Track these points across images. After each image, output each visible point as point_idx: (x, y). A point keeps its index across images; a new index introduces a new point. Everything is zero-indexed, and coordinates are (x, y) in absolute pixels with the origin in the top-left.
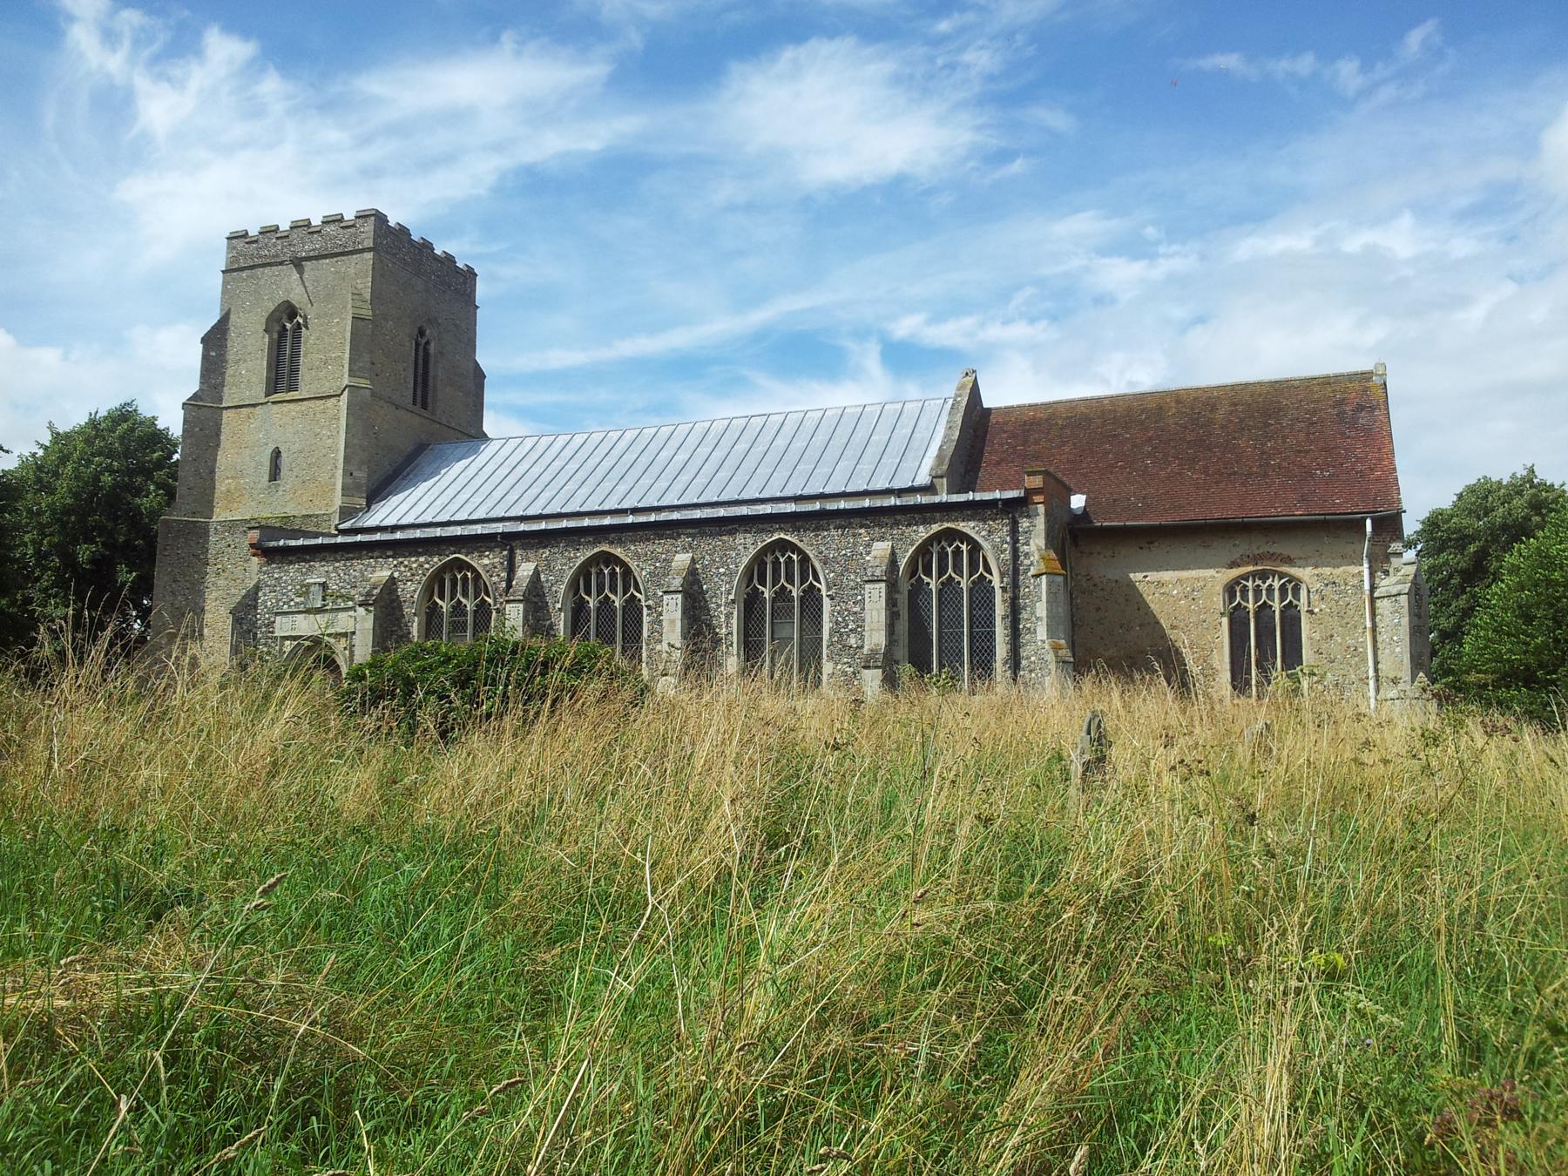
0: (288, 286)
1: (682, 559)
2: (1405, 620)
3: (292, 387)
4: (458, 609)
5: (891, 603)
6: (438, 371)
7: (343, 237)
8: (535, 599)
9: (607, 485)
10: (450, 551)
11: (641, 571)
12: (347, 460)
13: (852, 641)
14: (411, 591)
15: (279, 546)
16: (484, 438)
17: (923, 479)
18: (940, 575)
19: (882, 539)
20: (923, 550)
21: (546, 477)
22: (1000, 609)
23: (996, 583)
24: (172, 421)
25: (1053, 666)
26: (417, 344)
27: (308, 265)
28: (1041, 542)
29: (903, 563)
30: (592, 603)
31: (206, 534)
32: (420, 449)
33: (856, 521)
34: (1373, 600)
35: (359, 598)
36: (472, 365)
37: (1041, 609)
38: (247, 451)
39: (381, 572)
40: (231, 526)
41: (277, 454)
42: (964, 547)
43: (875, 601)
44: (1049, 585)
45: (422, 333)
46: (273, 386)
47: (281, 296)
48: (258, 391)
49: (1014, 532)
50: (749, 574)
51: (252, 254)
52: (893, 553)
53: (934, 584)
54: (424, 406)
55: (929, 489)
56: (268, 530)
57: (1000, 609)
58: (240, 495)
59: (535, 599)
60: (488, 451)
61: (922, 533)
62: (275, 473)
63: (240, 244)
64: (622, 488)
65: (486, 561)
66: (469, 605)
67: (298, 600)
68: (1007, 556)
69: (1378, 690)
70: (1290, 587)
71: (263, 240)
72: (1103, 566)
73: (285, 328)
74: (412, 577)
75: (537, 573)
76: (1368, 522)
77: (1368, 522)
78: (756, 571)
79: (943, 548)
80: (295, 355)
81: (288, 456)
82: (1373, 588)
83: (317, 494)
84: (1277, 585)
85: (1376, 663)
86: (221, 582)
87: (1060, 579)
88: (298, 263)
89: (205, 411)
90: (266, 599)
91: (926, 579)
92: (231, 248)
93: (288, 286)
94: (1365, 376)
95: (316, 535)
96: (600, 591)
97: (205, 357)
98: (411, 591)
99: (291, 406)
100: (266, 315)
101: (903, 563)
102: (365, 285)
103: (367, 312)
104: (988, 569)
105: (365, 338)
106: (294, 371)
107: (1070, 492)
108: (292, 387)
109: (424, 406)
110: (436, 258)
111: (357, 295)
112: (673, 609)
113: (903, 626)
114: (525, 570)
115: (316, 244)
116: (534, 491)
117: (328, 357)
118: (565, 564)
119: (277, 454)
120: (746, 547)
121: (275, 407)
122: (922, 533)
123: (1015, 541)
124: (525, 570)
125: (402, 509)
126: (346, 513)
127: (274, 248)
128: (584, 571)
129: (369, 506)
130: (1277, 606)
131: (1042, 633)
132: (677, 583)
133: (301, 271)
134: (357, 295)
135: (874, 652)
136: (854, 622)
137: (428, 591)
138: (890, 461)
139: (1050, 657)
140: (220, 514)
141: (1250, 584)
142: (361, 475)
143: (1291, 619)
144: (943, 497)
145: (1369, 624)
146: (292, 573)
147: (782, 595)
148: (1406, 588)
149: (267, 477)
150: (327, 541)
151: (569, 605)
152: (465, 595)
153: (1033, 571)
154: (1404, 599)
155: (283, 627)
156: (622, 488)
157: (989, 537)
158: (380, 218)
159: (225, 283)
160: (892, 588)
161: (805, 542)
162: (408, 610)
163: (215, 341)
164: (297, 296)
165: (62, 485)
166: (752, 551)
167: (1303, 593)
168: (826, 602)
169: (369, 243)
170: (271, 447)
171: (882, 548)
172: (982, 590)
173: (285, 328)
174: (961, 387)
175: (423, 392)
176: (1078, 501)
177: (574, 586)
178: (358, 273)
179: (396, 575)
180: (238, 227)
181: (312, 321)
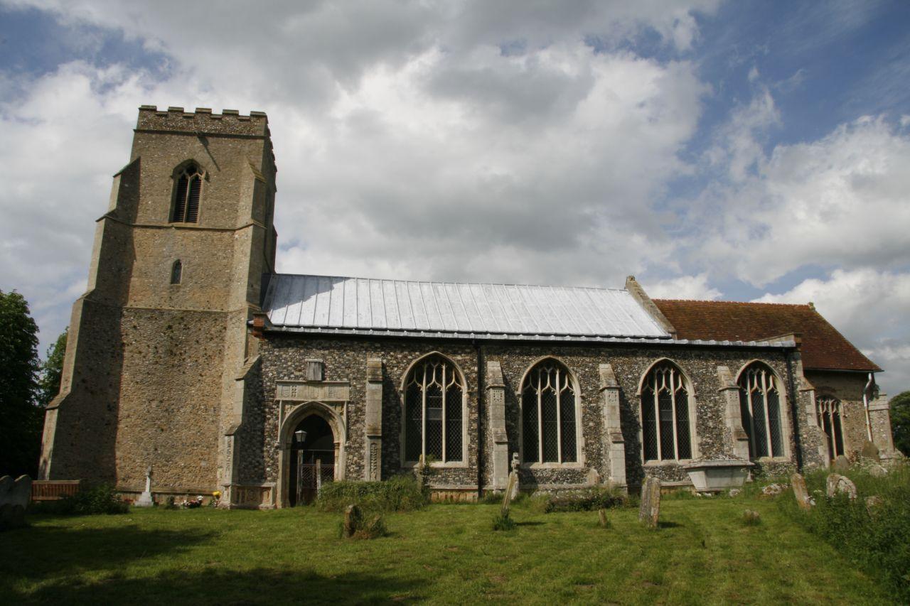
3: (191, 217)
7: (239, 128)
13: (711, 424)
33: (706, 353)
36: (272, 228)
38: (152, 259)
41: (177, 266)
46: (176, 216)
47: (186, 156)
48: (162, 217)
49: (789, 367)
53: (424, 389)
61: (534, 362)
62: (175, 278)
63: (151, 116)
65: (459, 358)
67: (298, 373)
70: (836, 403)
71: (171, 116)
79: (544, 370)
84: (830, 402)
88: (203, 137)
90: (270, 371)
91: (419, 385)
99: (192, 232)
108: (194, 221)
115: (218, 126)
119: (177, 266)
121: (179, 232)
122: (416, 358)
127: (180, 123)
133: (206, 144)
140: (130, 304)
145: (868, 423)
148: (887, 407)
149: (168, 280)
154: (886, 412)
155: (283, 393)
163: (129, 178)
164: (201, 156)
170: (174, 259)
177: (410, 378)
179: (385, 361)
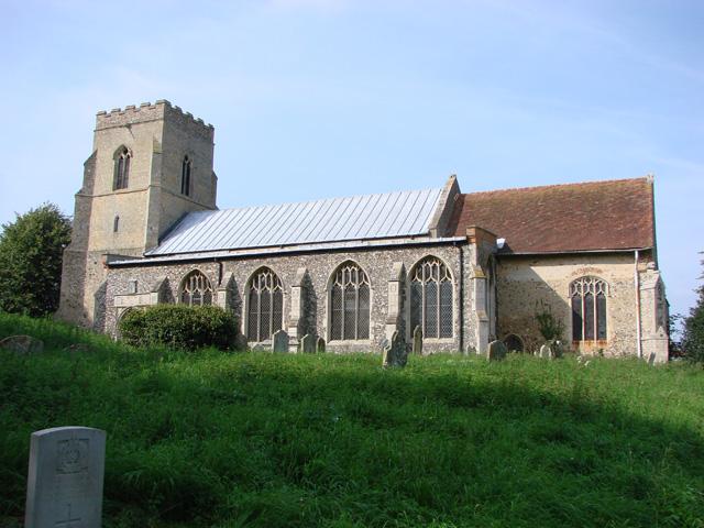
0: (125, 138)
1: (301, 271)
2: (653, 301)
3: (125, 186)
4: (197, 295)
5: (402, 292)
6: (194, 176)
8: (232, 289)
9: (271, 233)
10: (193, 268)
11: (283, 276)
12: (149, 222)
13: (383, 311)
14: (175, 285)
15: (116, 263)
16: (216, 209)
17: (425, 231)
18: (426, 278)
19: (398, 260)
20: (418, 266)
21: (243, 229)
22: (455, 295)
23: (453, 283)
24: (67, 209)
25: (478, 323)
26: (184, 164)
27: (133, 127)
28: (475, 262)
29: (408, 272)
30: (259, 292)
31: (85, 258)
32: (185, 215)
34: (639, 292)
35: (152, 289)
37: (474, 295)
39: (160, 274)
40: (95, 252)
41: (118, 218)
42: (438, 265)
43: (394, 289)
44: (477, 284)
45: (186, 158)
50: (334, 277)
51: (108, 122)
52: (403, 267)
54: (187, 194)
55: (428, 235)
56: (111, 256)
57: (455, 295)
58: (100, 240)
59: (232, 289)
60: (218, 214)
61: (417, 256)
64: (278, 235)
65: (209, 271)
66: (271, 291)
68: (458, 269)
69: (641, 335)
72: (515, 274)
73: (123, 157)
74: (175, 276)
75: (233, 277)
76: (636, 253)
77: (636, 253)
78: (337, 275)
80: (127, 170)
81: (120, 220)
82: (639, 286)
83: (136, 239)
84: (594, 284)
85: (640, 322)
86: (92, 281)
87: (483, 281)
88: (129, 126)
89: (84, 198)
90: (110, 288)
92: (98, 120)
93: (125, 138)
94: (643, 181)
95: (133, 258)
96: (427, 276)
97: (85, 173)
98: (175, 285)
100: (113, 152)
101: (408, 272)
102: (159, 137)
103: (160, 150)
104: (449, 275)
105: (161, 157)
106: (126, 178)
107: (496, 237)
109: (187, 194)
110: (194, 122)
111: (155, 141)
112: (296, 294)
113: (408, 304)
114: (227, 276)
115: (136, 117)
116: (237, 236)
117: (142, 171)
118: (243, 273)
120: (332, 263)
122: (417, 256)
123: (462, 262)
124: (227, 276)
125: (177, 244)
126: (148, 247)
127: (117, 119)
128: (255, 276)
129: (159, 245)
130: (594, 295)
131: (474, 307)
132: (298, 282)
134: (155, 141)
135: (391, 318)
136: (382, 302)
137: (183, 285)
138: (411, 221)
139: (477, 319)
140: (91, 248)
141: (582, 283)
142: (156, 229)
143: (601, 303)
144: (435, 240)
146: (122, 274)
147: (350, 288)
150: (140, 261)
151: (248, 293)
152: (269, 285)
153: (471, 276)
155: (118, 302)
156: (278, 235)
157: (448, 258)
158: (167, 104)
159: (95, 136)
160: (402, 284)
161: (361, 260)
162: (174, 294)
163: (90, 164)
165: (58, 362)
166: (335, 266)
167: (607, 287)
168: (371, 291)
169: (162, 116)
171: (398, 266)
172: (446, 289)
173: (123, 157)
174: (448, 184)
175: (186, 186)
176: (501, 241)
177: (250, 283)
178: (156, 130)
180: (102, 110)
181: (134, 152)
